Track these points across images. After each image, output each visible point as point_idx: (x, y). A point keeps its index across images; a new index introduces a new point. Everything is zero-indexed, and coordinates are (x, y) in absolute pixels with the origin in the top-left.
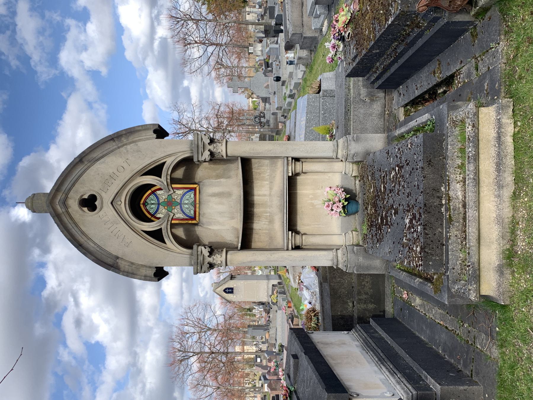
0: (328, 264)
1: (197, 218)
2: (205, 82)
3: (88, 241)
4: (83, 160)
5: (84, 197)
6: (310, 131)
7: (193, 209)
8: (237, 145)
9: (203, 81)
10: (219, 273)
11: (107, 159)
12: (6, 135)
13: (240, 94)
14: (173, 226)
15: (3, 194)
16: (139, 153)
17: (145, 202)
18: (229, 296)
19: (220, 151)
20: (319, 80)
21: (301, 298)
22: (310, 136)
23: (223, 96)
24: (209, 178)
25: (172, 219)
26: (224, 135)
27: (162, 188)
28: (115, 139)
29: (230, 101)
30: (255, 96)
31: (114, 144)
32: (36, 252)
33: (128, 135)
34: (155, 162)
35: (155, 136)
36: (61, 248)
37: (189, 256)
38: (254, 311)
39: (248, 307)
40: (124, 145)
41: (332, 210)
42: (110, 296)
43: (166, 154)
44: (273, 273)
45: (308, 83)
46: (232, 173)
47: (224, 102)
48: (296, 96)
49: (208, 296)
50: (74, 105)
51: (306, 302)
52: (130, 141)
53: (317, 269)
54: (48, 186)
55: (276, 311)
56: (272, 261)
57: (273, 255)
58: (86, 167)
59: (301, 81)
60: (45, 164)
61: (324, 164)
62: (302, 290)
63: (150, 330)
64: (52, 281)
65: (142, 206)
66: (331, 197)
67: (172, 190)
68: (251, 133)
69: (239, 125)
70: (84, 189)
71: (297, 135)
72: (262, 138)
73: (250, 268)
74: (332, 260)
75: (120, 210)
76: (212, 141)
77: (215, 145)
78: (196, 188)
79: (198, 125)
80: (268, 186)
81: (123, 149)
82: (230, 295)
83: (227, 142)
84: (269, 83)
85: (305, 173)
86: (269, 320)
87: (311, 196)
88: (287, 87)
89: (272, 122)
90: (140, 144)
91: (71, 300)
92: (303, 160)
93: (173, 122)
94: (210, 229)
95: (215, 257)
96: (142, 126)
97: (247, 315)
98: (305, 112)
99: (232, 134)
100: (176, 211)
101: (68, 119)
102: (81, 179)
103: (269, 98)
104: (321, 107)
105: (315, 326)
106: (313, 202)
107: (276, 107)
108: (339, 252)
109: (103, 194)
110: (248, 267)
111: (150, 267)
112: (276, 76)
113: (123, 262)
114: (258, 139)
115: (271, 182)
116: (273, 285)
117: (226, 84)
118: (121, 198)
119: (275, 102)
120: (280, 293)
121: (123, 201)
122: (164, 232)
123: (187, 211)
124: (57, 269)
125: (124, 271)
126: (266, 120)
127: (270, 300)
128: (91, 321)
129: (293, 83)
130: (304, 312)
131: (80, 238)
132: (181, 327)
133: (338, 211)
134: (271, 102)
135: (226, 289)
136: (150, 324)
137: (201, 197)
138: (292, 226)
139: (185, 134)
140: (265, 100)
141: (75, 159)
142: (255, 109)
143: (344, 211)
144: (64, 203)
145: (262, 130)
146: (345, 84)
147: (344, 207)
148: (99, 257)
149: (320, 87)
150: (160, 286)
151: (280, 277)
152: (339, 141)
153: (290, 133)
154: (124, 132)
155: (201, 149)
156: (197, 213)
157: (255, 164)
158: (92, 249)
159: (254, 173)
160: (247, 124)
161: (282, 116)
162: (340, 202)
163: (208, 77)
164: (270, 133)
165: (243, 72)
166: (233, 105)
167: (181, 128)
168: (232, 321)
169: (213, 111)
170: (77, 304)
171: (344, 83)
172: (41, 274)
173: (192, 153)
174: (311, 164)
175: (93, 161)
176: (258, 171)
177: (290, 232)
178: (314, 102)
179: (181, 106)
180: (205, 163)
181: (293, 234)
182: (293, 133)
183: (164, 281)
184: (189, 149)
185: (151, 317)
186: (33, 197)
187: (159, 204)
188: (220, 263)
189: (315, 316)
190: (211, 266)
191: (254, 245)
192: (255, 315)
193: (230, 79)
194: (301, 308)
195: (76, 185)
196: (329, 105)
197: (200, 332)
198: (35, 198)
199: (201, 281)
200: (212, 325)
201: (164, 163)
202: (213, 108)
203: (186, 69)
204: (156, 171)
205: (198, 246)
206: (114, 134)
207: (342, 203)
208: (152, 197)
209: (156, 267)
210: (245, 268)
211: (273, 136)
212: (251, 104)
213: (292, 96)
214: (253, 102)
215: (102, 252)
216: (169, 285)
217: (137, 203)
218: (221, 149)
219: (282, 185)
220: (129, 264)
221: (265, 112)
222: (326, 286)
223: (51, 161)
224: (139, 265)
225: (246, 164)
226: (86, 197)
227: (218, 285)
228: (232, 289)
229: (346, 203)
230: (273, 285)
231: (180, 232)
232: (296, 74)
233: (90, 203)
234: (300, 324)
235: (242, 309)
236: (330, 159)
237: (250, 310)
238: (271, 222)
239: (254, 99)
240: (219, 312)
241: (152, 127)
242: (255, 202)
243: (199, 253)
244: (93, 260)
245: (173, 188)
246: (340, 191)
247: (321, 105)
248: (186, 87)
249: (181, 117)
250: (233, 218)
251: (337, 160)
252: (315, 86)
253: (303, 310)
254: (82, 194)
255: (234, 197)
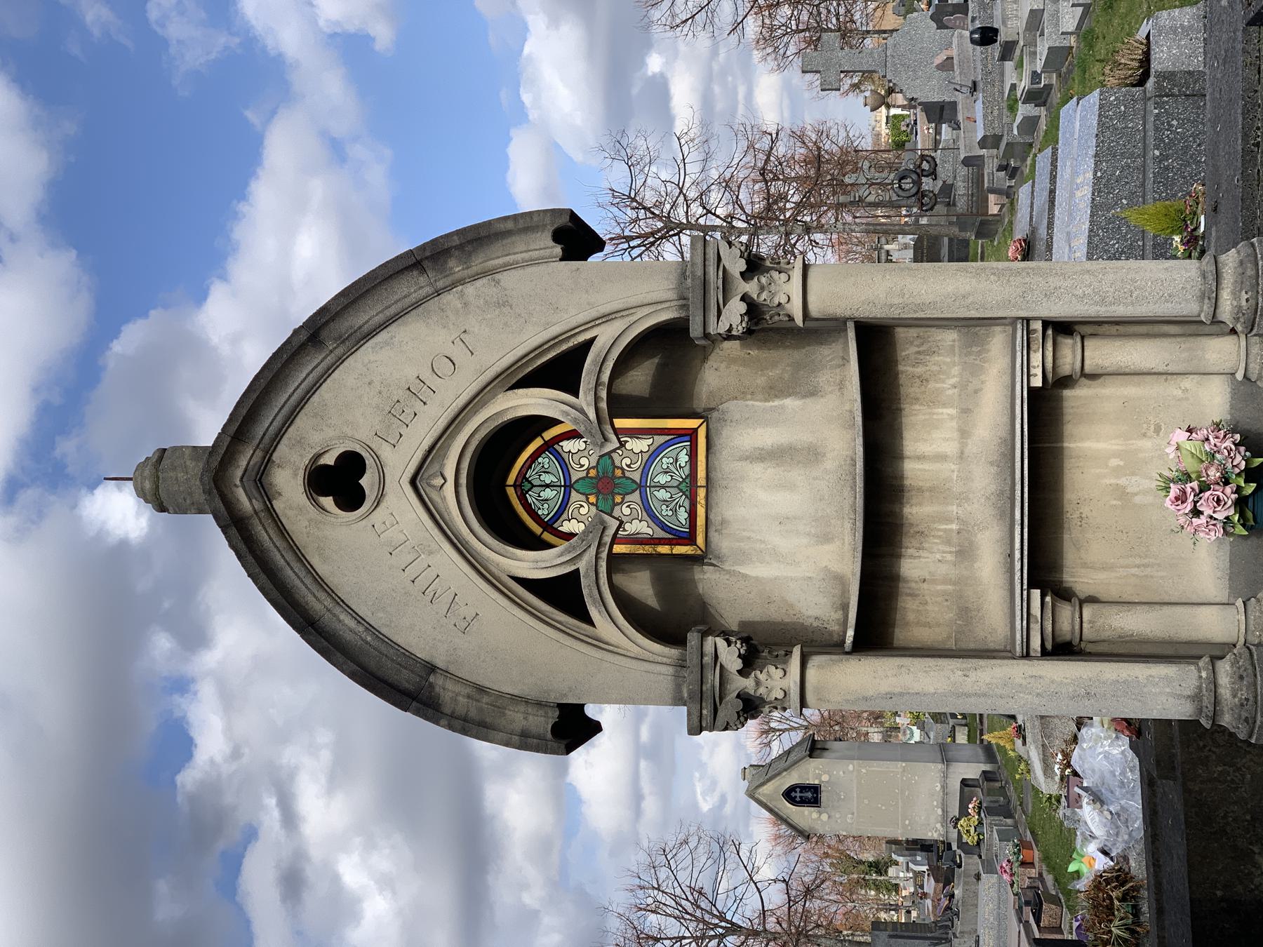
0: (1179, 710)
1: (700, 540)
2: (722, 56)
3: (337, 610)
4: (322, 338)
5: (322, 461)
6: (1109, 221)
7: (687, 504)
8: (836, 279)
9: (714, 53)
10: (766, 732)
11: (398, 332)
12: (74, 253)
13: (846, 93)
14: (616, 563)
15: (57, 453)
16: (506, 310)
17: (522, 475)
18: (805, 816)
19: (783, 300)
20: (1141, 35)
21: (1072, 832)
22: (1110, 240)
23: (786, 102)
24: (744, 393)
25: (615, 539)
26: (787, 240)
27: (581, 429)
28: (426, 264)
29: (809, 120)
30: (899, 99)
31: (422, 280)
32: (162, 643)
33: (468, 248)
34: (556, 340)
35: (558, 250)
36: (244, 627)
37: (671, 670)
38: (892, 871)
39: (869, 857)
40: (454, 285)
41: (1196, 513)
42: (400, 802)
43: (594, 313)
44: (962, 738)
45: (1101, 49)
46: (825, 378)
47: (787, 125)
48: (1056, 96)
49: (728, 809)
50: (285, 148)
51: (1092, 848)
52: (474, 269)
53: (1134, 728)
54: (207, 427)
55: (978, 877)
56: (968, 695)
57: (973, 675)
58: (329, 360)
59: (1072, 41)
60: (194, 348)
61: (1165, 343)
62: (1075, 802)
63: (529, 918)
64: (212, 741)
65: (511, 492)
66: (1190, 465)
67: (613, 437)
68: (886, 233)
69: (839, 207)
70: (321, 432)
71: (1058, 236)
72: (926, 252)
73: (877, 717)
74: (1196, 698)
75: (441, 506)
76: (754, 266)
77: (764, 280)
78: (695, 431)
79: (696, 209)
80: (954, 424)
81: (449, 298)
82: (806, 810)
83: (806, 268)
84: (954, 52)
85: (1093, 377)
86: (948, 908)
87: (1114, 462)
88: (1020, 66)
89: (961, 189)
90: (507, 278)
91: (271, 802)
92: (1087, 330)
93: (609, 198)
94: (745, 576)
95: (762, 677)
96: (515, 218)
97: (866, 884)
98: (1092, 152)
99: (818, 237)
100: (626, 511)
101: (266, 197)
102: (315, 398)
103: (954, 104)
104: (1151, 133)
105: (1126, 935)
106: (1122, 481)
107: (980, 135)
108: (1224, 667)
109: (386, 452)
110: (872, 713)
111: (540, 704)
112: (978, 24)
113: (450, 685)
114: (910, 253)
115: (966, 411)
116: (964, 783)
117: (798, 62)
118: (442, 466)
119: (976, 119)
120: (991, 811)
121: (450, 472)
122: (586, 584)
123: (664, 512)
124: (229, 701)
125: (452, 716)
126: (940, 183)
127: (953, 835)
128: (336, 879)
129: (1042, 49)
130: (1082, 885)
131: (310, 598)
132: (633, 917)
133: (1220, 516)
134: (960, 117)
135: (792, 789)
136: (530, 899)
137: (715, 462)
138: (1043, 566)
139: (652, 240)
140: (940, 113)
141: (296, 332)
142: (900, 145)
143: (1242, 516)
144: (260, 481)
145: (924, 221)
146: (1244, 51)
147: (1241, 503)
148: (372, 665)
149: (1146, 61)
150: (563, 771)
151: (990, 752)
152: (1222, 258)
153: (1034, 231)
154: (456, 241)
155: (715, 296)
156: (701, 521)
157: (907, 346)
158: (348, 636)
159: (903, 379)
160: (871, 199)
161: (1001, 168)
162: (1227, 483)
163: (734, 37)
164: (955, 230)
165: (857, 16)
166: (820, 133)
167: (637, 220)
168: (814, 905)
169: (749, 158)
170: (290, 819)
171: (1239, 46)
172: (177, 714)
173: (684, 307)
174: (1118, 343)
175: (353, 340)
176: (919, 370)
177: (1036, 593)
178: (1123, 117)
179: (641, 143)
180: (727, 344)
181: (1048, 599)
182: (1042, 232)
183: (579, 756)
184: (671, 295)
185: (532, 873)
186: (160, 459)
187: (568, 487)
188: (780, 695)
189: (1123, 899)
190: (750, 707)
191: (901, 636)
192: (896, 888)
193: (809, 42)
194: (1072, 868)
195: (298, 420)
196: (1181, 126)
197: (703, 937)
198: (165, 462)
199: (704, 757)
200: (746, 913)
201: (589, 344)
202: (751, 146)
203: (656, 14)
204: (560, 370)
205: (704, 635)
206: (423, 248)
207: (1234, 486)
208: (544, 460)
209: (561, 706)
210: (858, 716)
211: (965, 243)
212: (884, 130)
213: (1037, 96)
214: (893, 121)
215: (383, 648)
216: (593, 766)
217: (497, 482)
218: (785, 292)
219: (1006, 419)
220: (468, 690)
221: (938, 155)
222: (1171, 792)
223: (215, 340)
224: (501, 695)
225: (876, 343)
226: (329, 460)
227: (759, 775)
228: (815, 789)
229: (1250, 489)
230: (964, 783)
231: (641, 585)
232: (1056, 16)
233: (341, 481)
234: (1065, 927)
235: (848, 863)
236: (1188, 327)
237: (879, 867)
238: (965, 553)
239: (893, 111)
240: (766, 872)
241: (548, 220)
242: (907, 482)
243: (708, 659)
244: (352, 676)
245: (617, 432)
246: (1228, 443)
247: (1150, 126)
248: (654, 76)
249: (639, 183)
250: (826, 538)
251: (1215, 328)
252: (1130, 59)
253: (1077, 875)
254: (317, 449)
255: (830, 464)
